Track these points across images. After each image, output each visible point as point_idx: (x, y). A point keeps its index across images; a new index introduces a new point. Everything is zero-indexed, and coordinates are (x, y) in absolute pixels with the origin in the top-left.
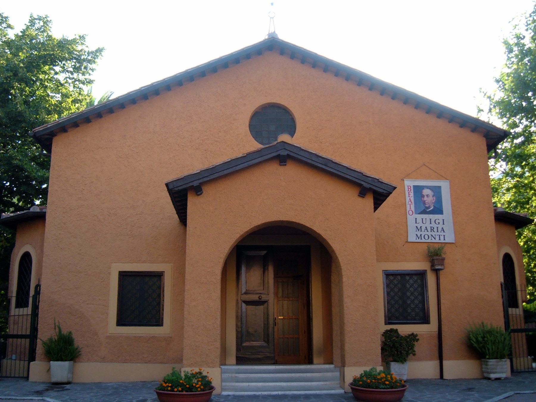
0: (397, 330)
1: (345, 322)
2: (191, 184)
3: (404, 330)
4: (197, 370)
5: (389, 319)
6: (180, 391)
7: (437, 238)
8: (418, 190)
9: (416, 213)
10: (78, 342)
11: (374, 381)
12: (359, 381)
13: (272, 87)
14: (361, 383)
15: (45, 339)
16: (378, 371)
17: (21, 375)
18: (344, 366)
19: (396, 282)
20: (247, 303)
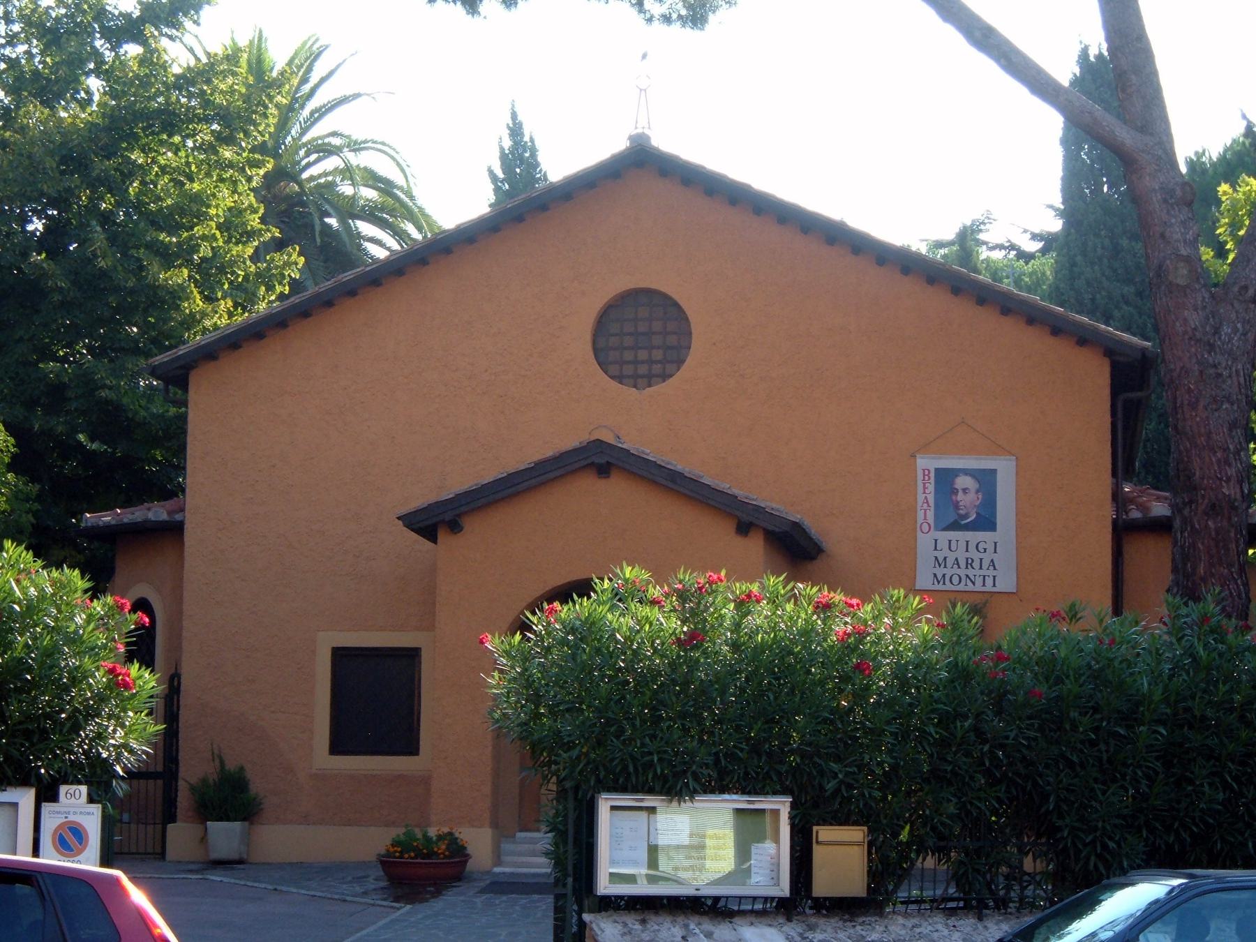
4: (446, 830)
7: (979, 581)
8: (945, 478)
9: (937, 529)
10: (257, 786)
15: (193, 780)
17: (150, 850)
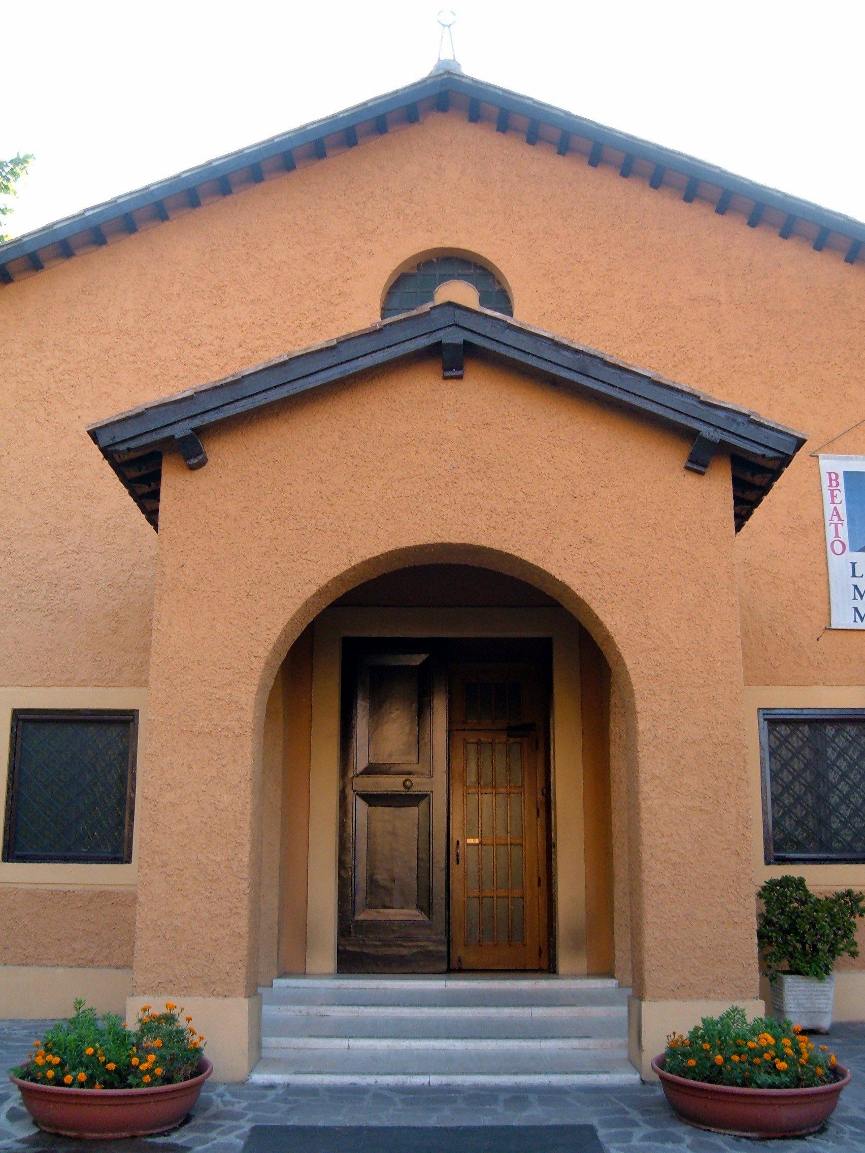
0: (801, 881)
1: (645, 857)
2: (166, 433)
3: (824, 879)
5: (777, 849)
6: (82, 1085)
9: (853, 549)
11: (736, 1058)
12: (686, 1055)
13: (443, 200)
14: (692, 1062)
16: (750, 1020)
18: (641, 998)
19: (795, 742)
20: (372, 799)
